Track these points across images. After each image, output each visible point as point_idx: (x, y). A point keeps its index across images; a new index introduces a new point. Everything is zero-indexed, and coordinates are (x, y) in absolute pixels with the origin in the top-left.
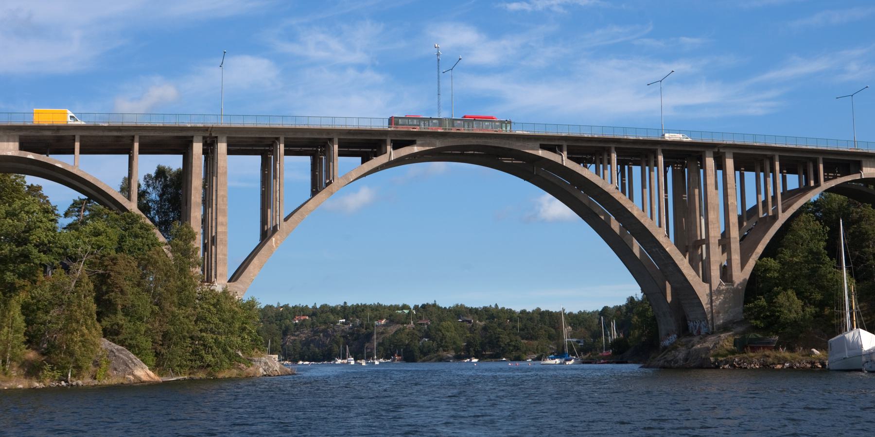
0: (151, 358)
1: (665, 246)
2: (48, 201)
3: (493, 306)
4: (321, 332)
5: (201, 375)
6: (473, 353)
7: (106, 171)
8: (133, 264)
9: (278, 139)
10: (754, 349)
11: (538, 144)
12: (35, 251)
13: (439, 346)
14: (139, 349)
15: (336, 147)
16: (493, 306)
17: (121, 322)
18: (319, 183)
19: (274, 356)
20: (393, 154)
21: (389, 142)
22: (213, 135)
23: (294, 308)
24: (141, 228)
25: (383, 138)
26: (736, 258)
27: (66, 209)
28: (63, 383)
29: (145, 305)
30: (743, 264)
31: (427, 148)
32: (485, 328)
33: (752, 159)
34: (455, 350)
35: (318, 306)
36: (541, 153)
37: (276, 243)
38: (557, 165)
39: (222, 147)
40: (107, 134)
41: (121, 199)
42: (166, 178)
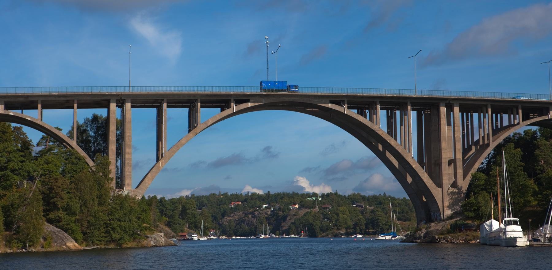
0: (80, 236)
1: (412, 164)
2: (26, 136)
3: (382, 194)
4: (250, 214)
5: (112, 246)
6: (358, 231)
8: (67, 181)
9: (163, 100)
10: (461, 231)
11: (328, 100)
12: (10, 174)
13: (335, 225)
14: (72, 231)
15: (199, 104)
16: (382, 194)
17: (60, 215)
18: (192, 124)
19: (161, 234)
20: (234, 108)
21: (232, 100)
22: (123, 98)
23: (231, 195)
24: (76, 158)
25: (229, 98)
26: (460, 171)
27: (38, 141)
28: (24, 250)
29: (76, 205)
30: (464, 177)
31: (257, 104)
32: (372, 212)
33: (470, 106)
34: (346, 229)
36: (330, 106)
37: (162, 164)
38: (346, 112)
39: (128, 106)
40: (57, 99)
42: (98, 122)
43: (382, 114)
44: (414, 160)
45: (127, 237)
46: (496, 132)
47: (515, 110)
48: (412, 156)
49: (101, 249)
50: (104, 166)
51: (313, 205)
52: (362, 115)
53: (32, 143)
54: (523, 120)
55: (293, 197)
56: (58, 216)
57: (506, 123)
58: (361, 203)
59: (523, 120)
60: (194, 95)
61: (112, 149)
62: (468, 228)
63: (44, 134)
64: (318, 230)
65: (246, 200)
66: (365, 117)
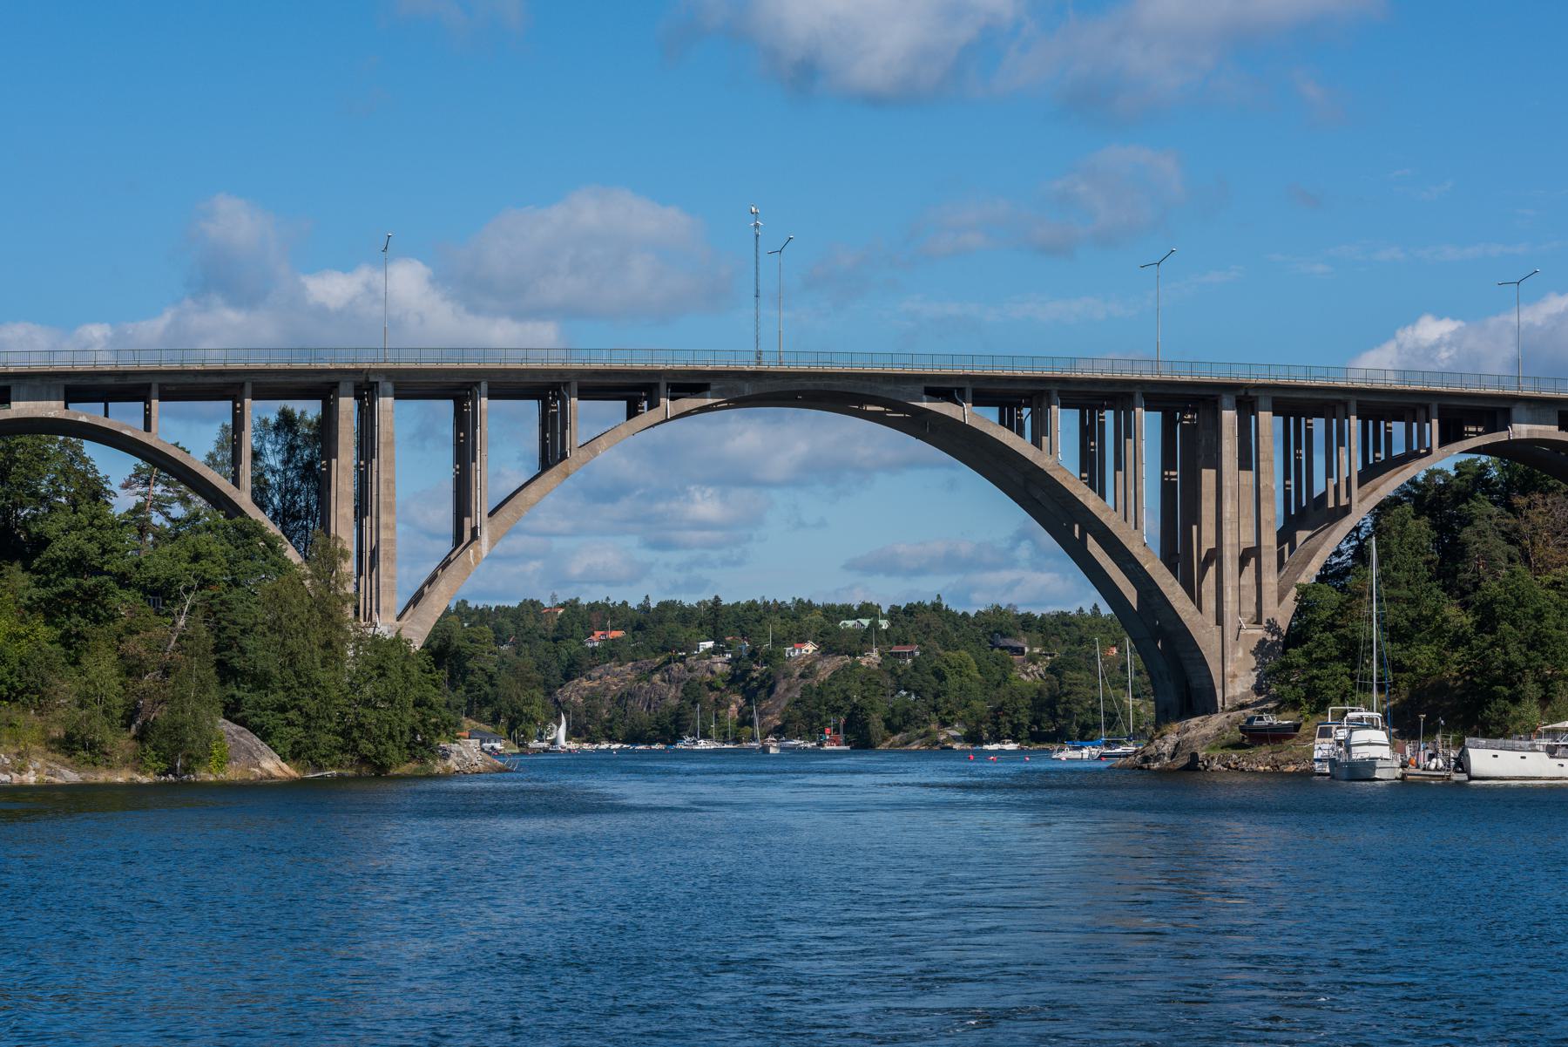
1: (1142, 562)
3: (1087, 611)
7: (192, 433)
11: (921, 387)
16: (1087, 611)
18: (551, 454)
33: (1297, 404)
35: (653, 605)
40: (200, 380)
41: (224, 485)
43: (1064, 422)
44: (1149, 550)
45: (394, 754)
46: (1370, 472)
47: (1422, 414)
48: (1143, 536)
49: (341, 777)
50: (325, 558)
51: (865, 639)
52: (1010, 428)
53: (108, 487)
54: (1442, 443)
55: (795, 618)
56: (233, 696)
57: (1399, 449)
58: (1017, 638)
59: (1442, 443)
60: (561, 372)
61: (344, 516)
62: (1276, 736)
63: (139, 461)
64: (876, 724)
65: (640, 627)
66: (1021, 433)
